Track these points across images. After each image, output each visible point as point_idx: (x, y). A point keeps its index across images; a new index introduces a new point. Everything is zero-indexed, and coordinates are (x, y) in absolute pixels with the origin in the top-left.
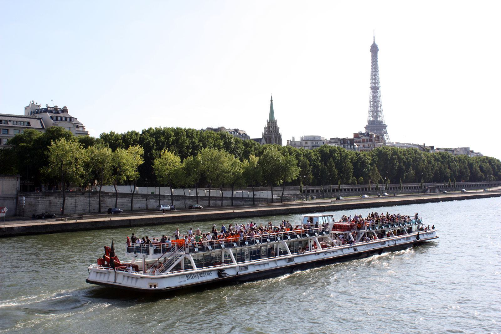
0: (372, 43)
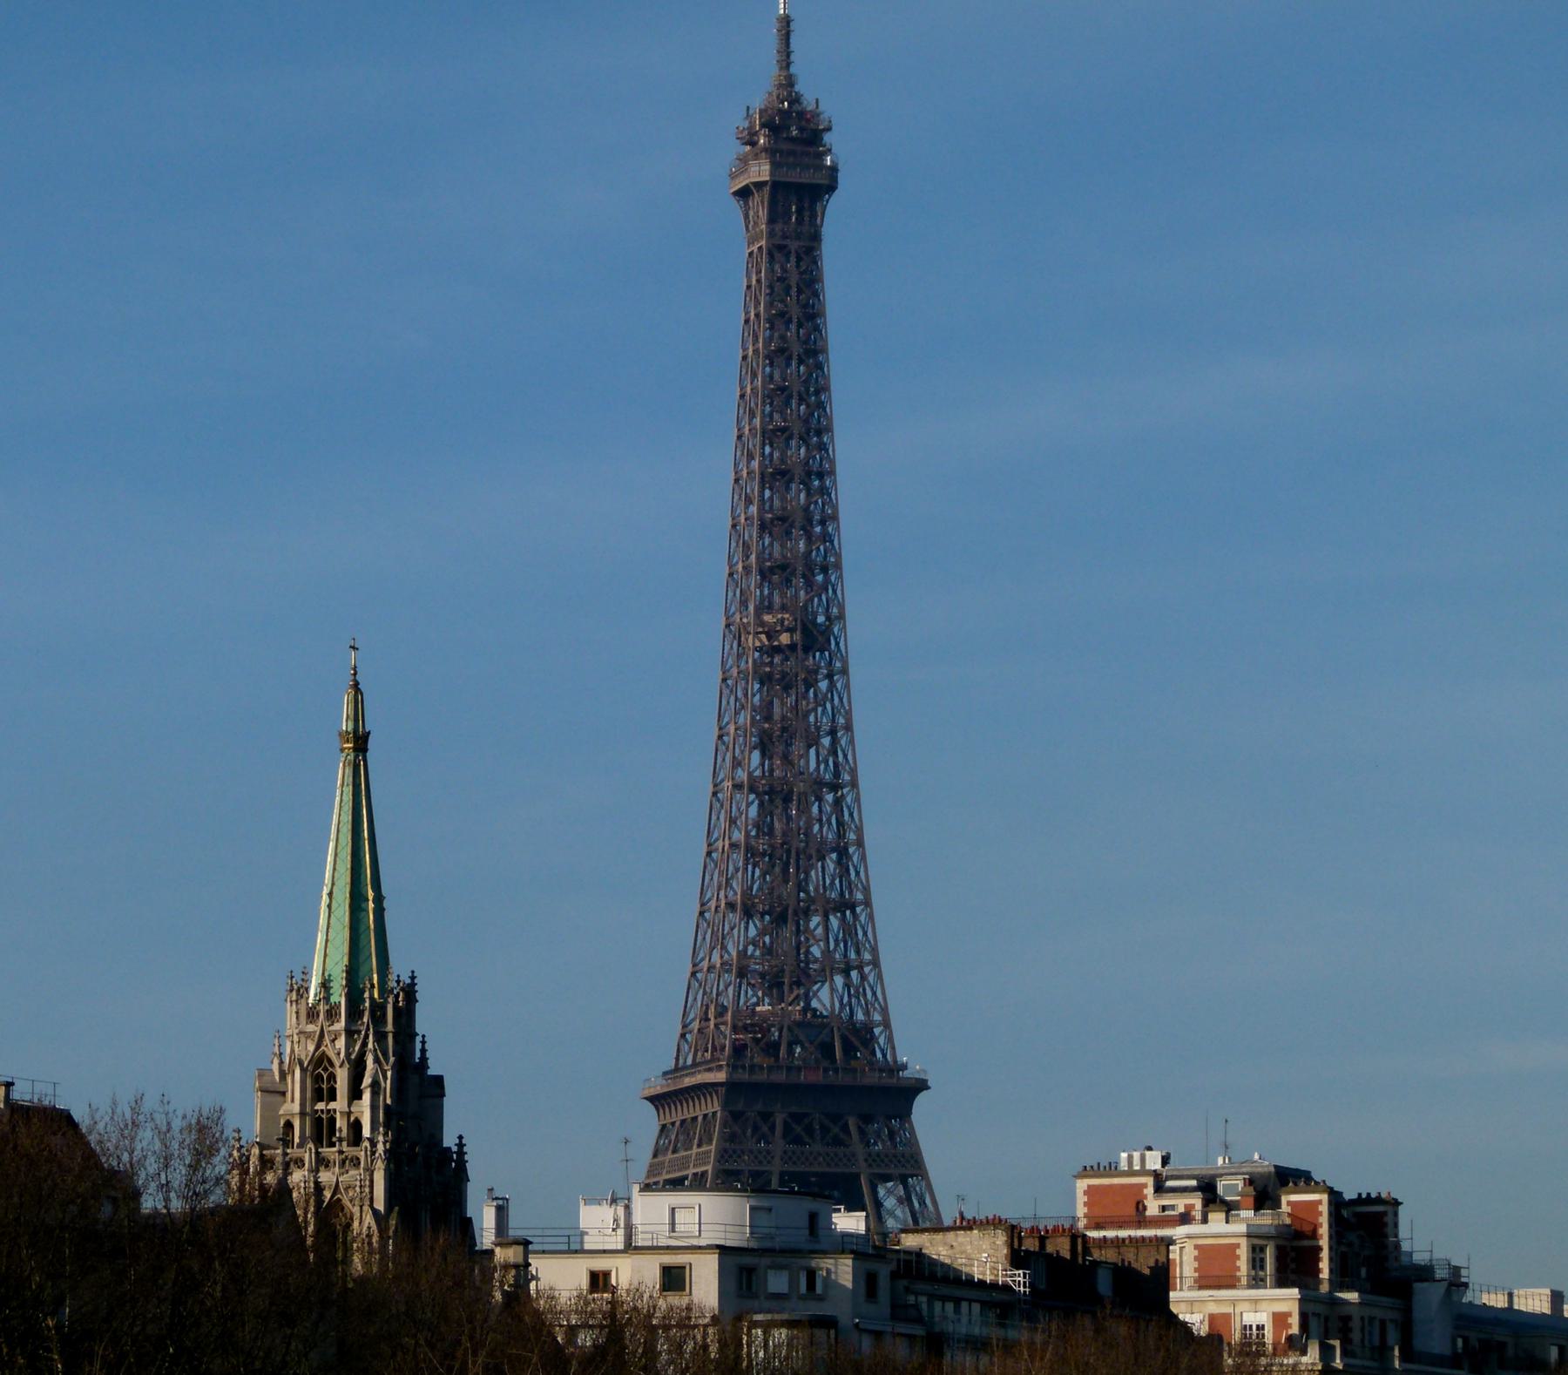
0: (759, 94)
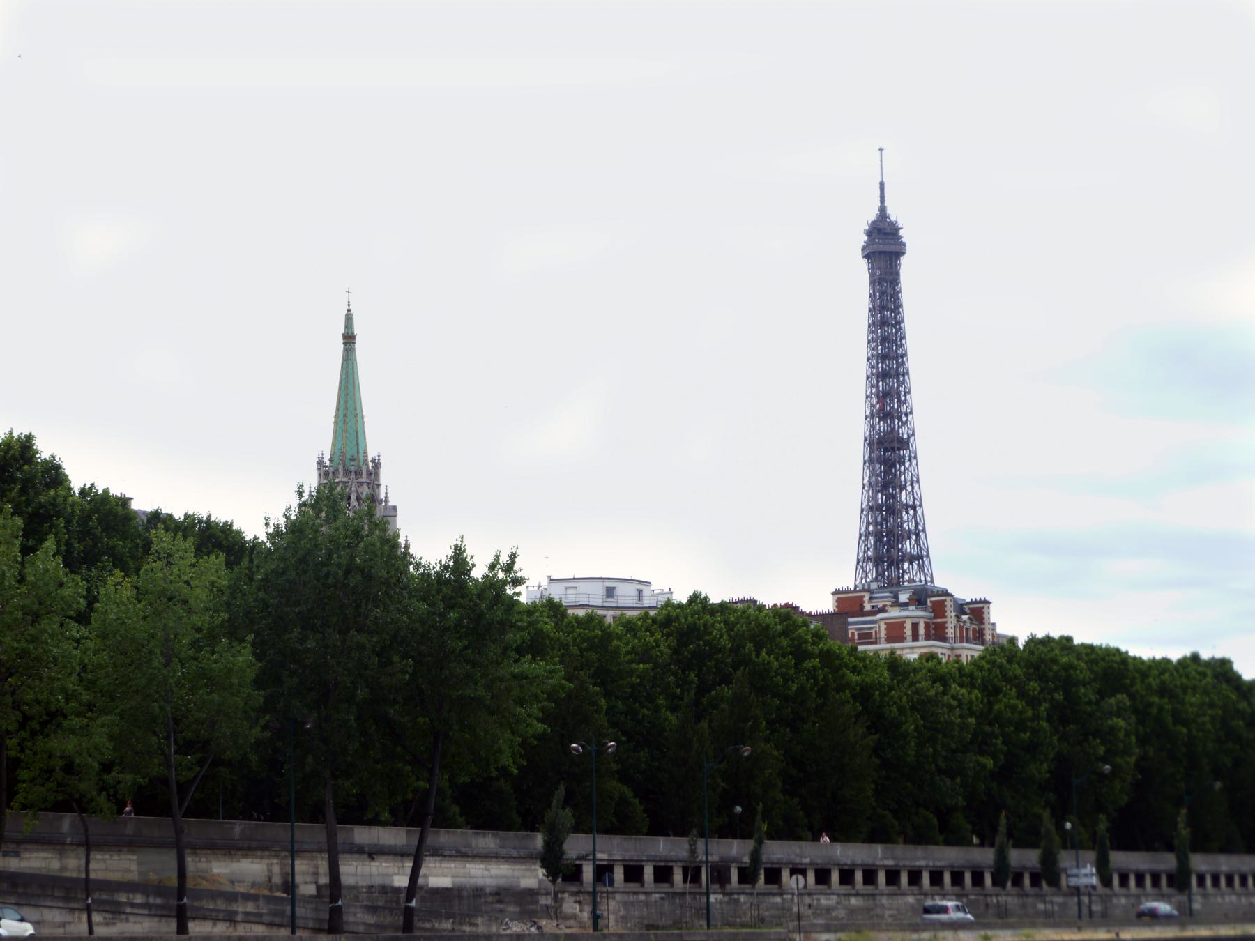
0: (873, 215)
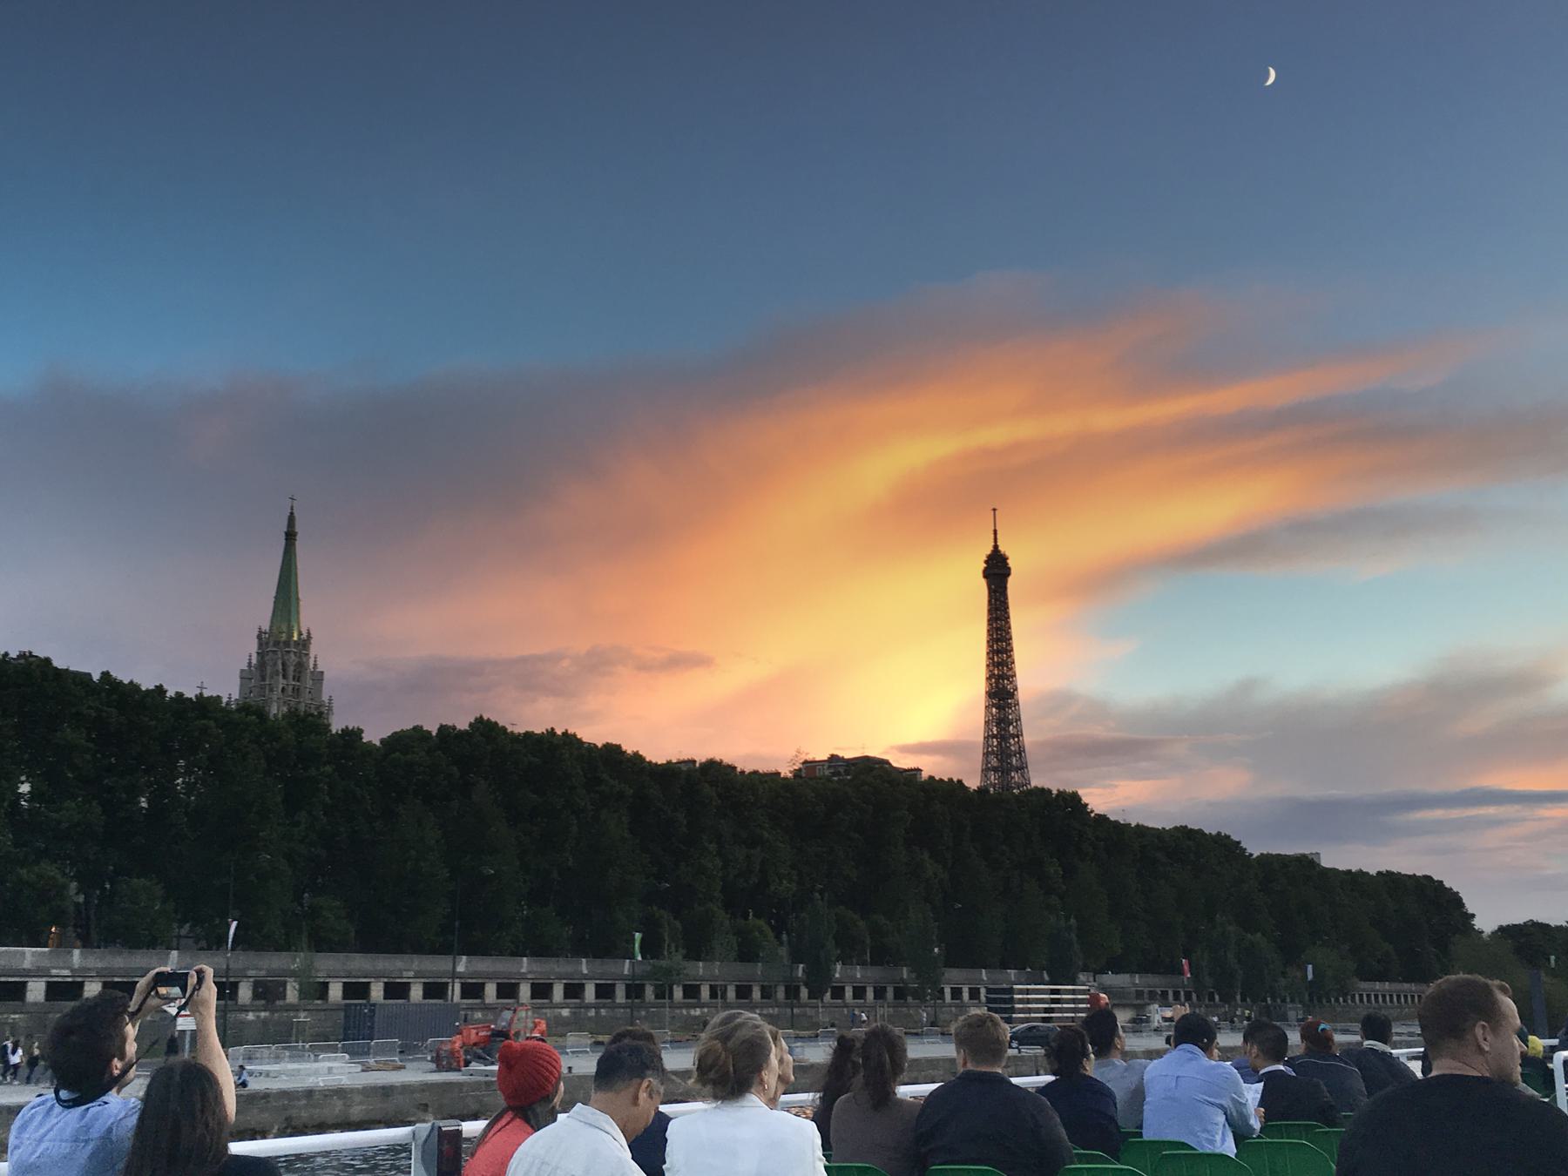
0: (989, 550)
